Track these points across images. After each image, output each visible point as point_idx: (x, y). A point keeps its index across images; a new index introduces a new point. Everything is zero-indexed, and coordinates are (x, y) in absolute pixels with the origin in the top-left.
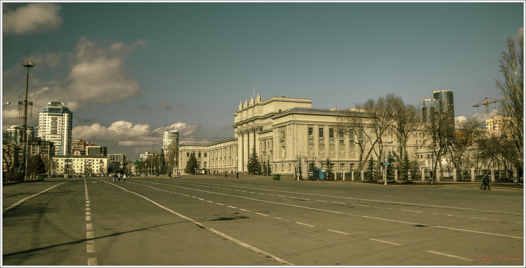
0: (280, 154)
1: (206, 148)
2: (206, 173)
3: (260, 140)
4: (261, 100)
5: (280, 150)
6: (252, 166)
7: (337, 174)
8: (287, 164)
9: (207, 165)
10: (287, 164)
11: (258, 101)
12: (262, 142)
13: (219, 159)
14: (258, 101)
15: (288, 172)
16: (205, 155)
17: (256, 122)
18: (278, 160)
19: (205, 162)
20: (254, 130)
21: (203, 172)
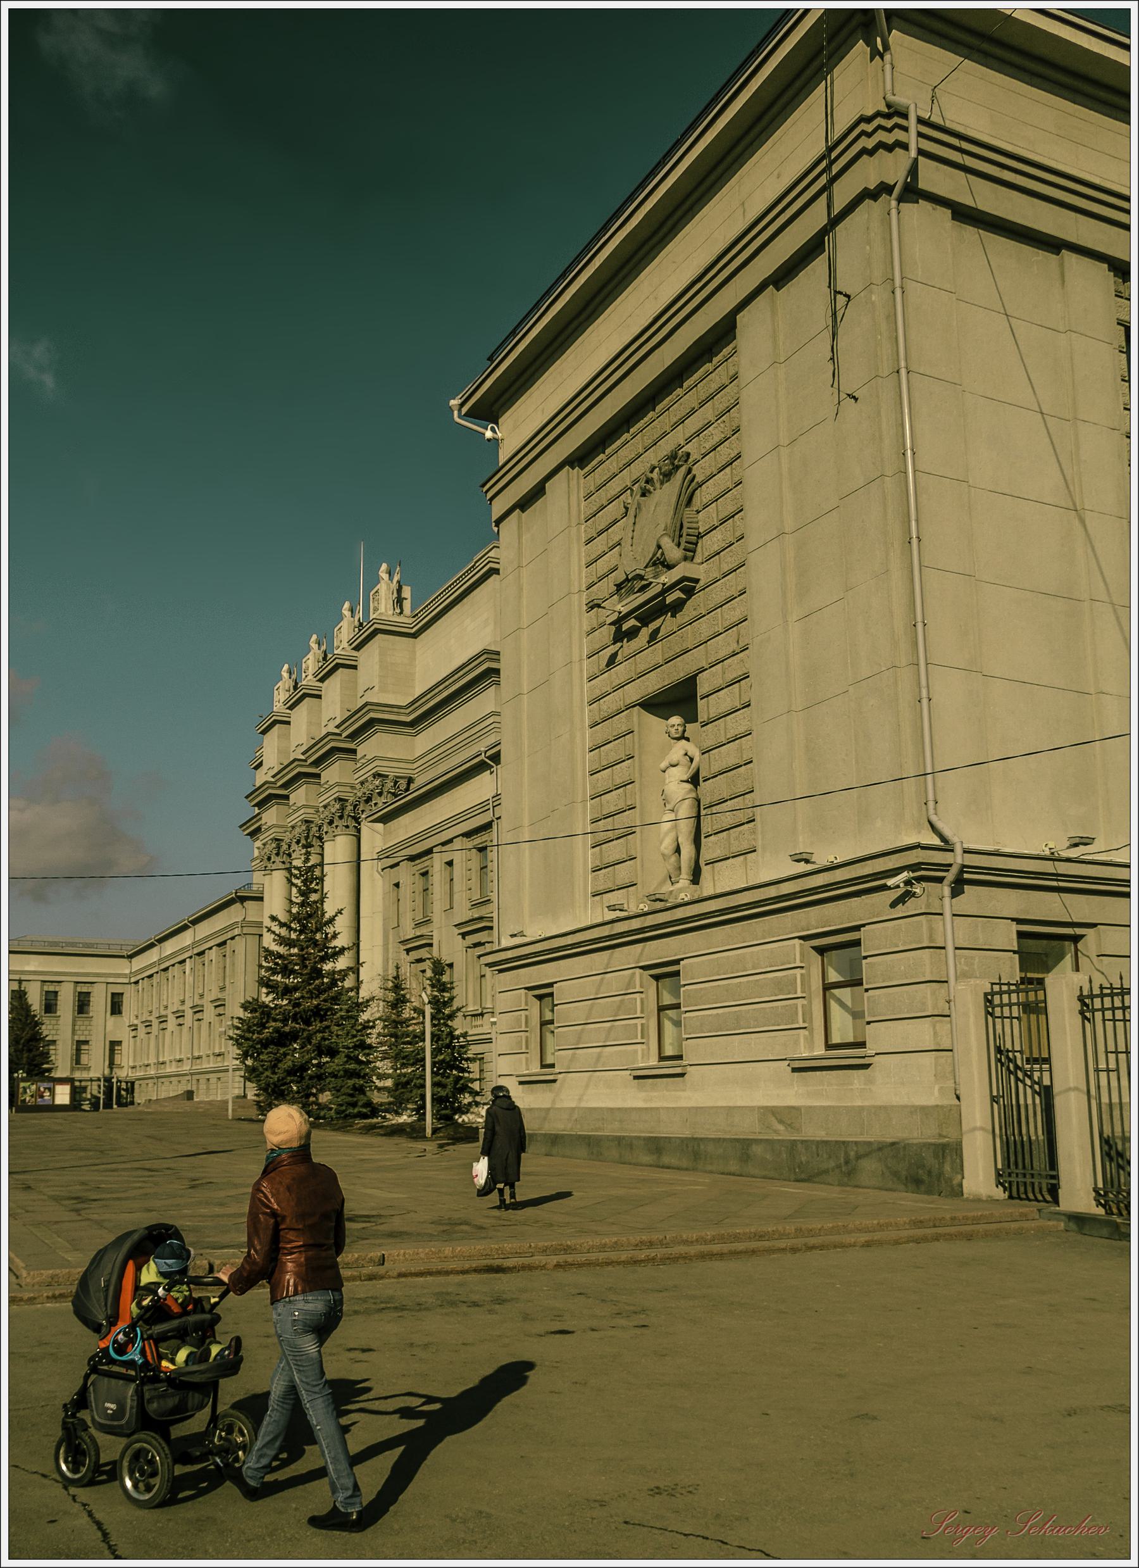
0: (615, 828)
1: (123, 967)
2: (75, 1104)
3: (390, 860)
4: (400, 601)
5: (614, 762)
6: (282, 1039)
7: (112, 1108)
8: (780, 945)
9: (125, 1058)
10: (780, 945)
11: (383, 608)
12: (406, 874)
13: (172, 1022)
14: (383, 608)
15: (634, 1097)
16: (116, 1007)
17: (368, 748)
18: (585, 914)
19: (114, 1045)
20: (349, 814)
21: (63, 1095)
